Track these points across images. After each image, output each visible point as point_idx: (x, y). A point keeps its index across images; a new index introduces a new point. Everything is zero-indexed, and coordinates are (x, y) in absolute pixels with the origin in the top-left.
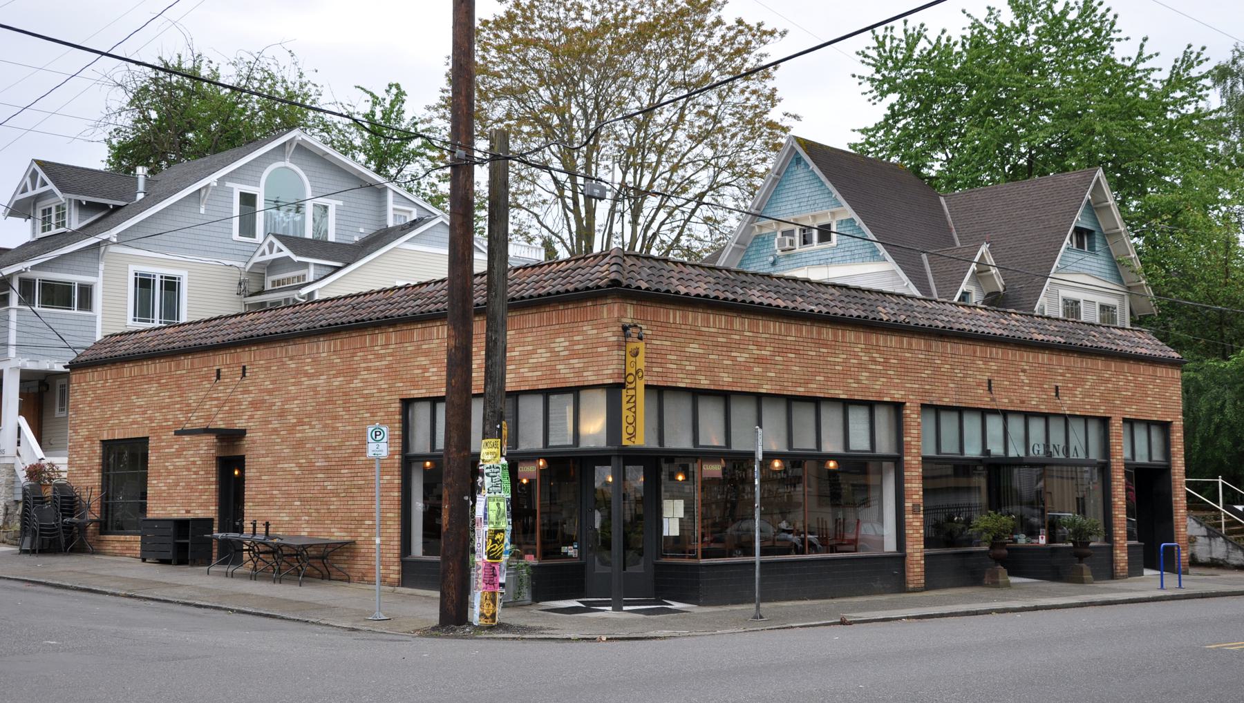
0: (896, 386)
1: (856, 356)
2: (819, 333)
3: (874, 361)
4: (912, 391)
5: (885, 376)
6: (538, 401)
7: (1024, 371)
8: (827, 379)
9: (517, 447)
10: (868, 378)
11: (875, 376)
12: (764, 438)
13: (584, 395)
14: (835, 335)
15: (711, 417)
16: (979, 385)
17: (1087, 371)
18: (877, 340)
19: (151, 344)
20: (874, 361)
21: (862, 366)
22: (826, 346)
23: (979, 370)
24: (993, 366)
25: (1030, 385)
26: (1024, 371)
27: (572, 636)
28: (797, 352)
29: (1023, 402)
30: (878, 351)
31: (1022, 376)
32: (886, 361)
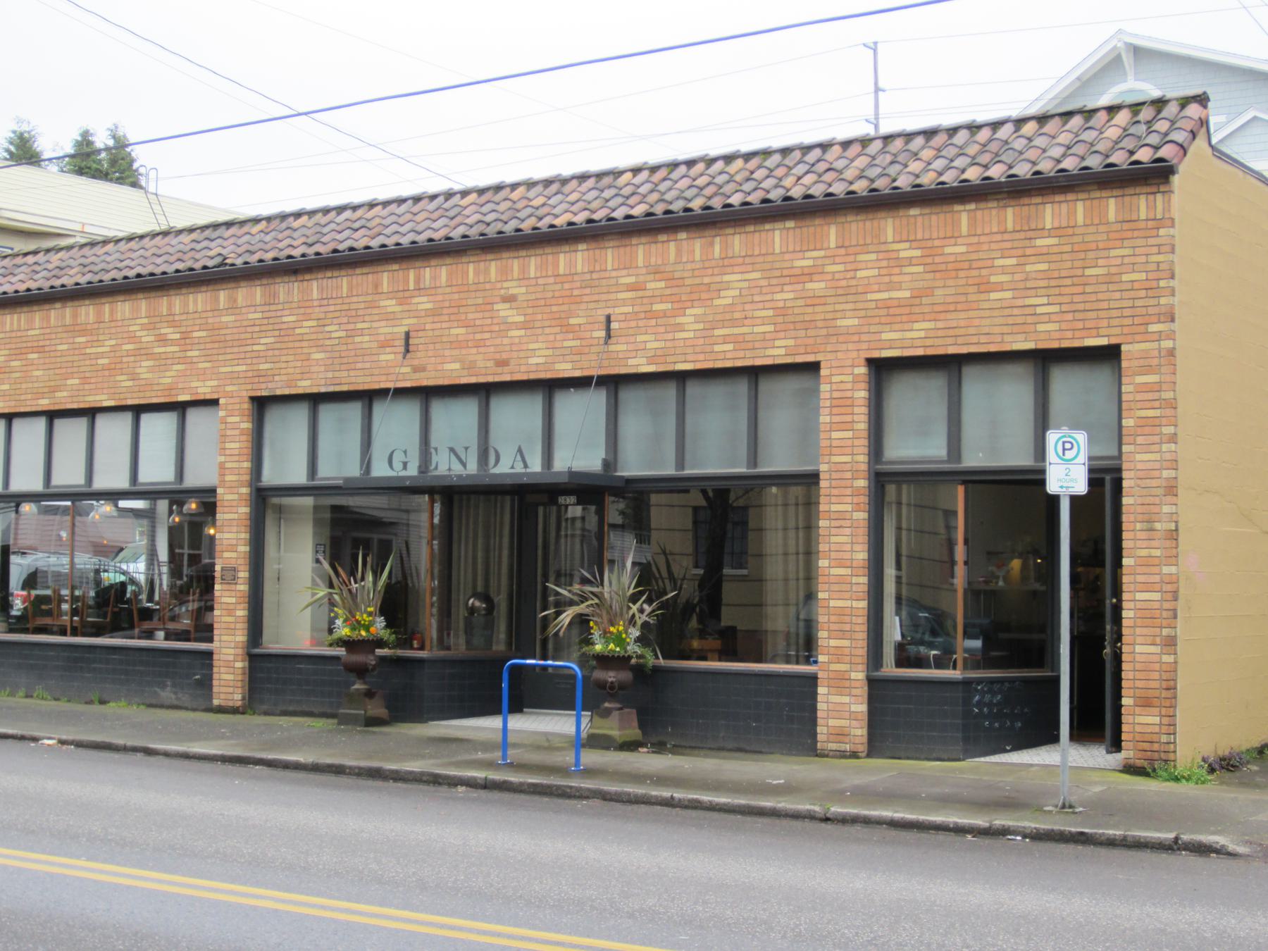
0: (203, 376)
1: (132, 338)
2: (75, 316)
3: (162, 340)
4: (233, 377)
5: (184, 360)
6: (597, 400)
7: (509, 299)
8: (85, 380)
9: (755, 465)
10: (151, 370)
11: (163, 363)
12: (395, 448)
13: (101, 421)
14: (99, 313)
15: (580, 419)
16: (383, 345)
17: (727, 263)
18: (170, 306)
19: (631, 362)
20: (162, 340)
21: (142, 352)
22: (83, 332)
23: (390, 318)
24: (423, 303)
25: (524, 326)
26: (509, 299)
27: (316, 711)
28: (40, 350)
29: (502, 363)
30: (173, 324)
31: (503, 310)
32: (185, 336)
